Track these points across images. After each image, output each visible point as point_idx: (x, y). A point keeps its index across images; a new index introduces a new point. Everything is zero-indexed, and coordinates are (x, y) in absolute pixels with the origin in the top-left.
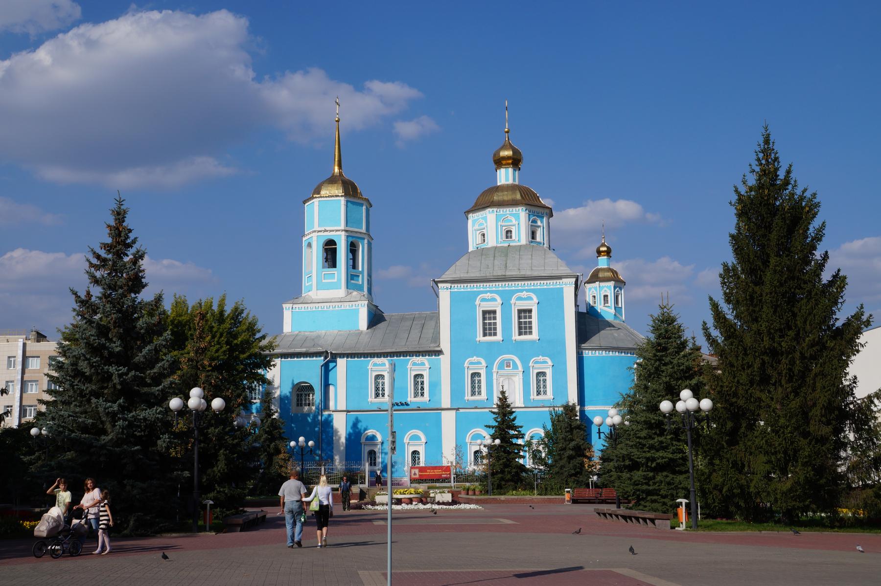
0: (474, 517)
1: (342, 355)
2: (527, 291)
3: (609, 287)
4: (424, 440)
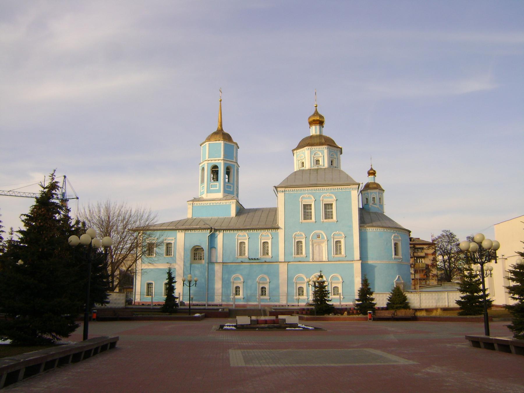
0: (200, 305)
1: (219, 230)
3: (376, 193)
4: (242, 280)
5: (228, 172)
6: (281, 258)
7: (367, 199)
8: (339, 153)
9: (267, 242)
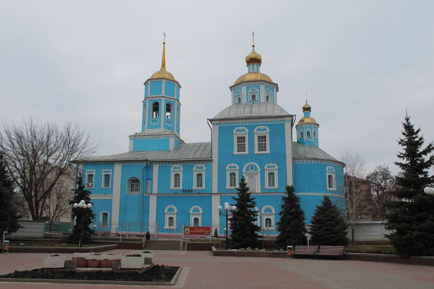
2: (264, 125)
4: (176, 211)
5: (168, 108)
6: (215, 190)
7: (302, 133)
8: (275, 90)
9: (201, 174)
